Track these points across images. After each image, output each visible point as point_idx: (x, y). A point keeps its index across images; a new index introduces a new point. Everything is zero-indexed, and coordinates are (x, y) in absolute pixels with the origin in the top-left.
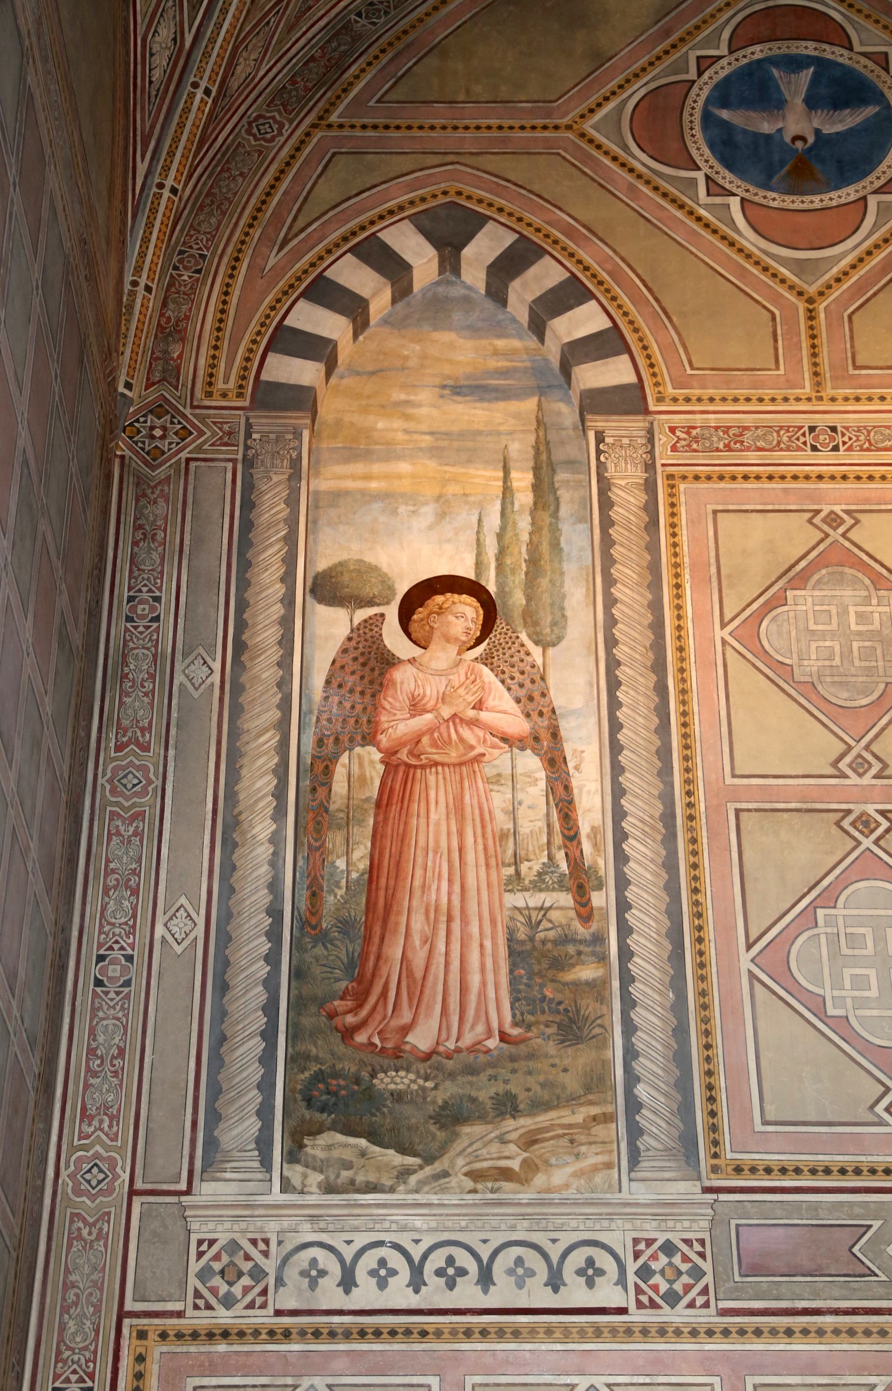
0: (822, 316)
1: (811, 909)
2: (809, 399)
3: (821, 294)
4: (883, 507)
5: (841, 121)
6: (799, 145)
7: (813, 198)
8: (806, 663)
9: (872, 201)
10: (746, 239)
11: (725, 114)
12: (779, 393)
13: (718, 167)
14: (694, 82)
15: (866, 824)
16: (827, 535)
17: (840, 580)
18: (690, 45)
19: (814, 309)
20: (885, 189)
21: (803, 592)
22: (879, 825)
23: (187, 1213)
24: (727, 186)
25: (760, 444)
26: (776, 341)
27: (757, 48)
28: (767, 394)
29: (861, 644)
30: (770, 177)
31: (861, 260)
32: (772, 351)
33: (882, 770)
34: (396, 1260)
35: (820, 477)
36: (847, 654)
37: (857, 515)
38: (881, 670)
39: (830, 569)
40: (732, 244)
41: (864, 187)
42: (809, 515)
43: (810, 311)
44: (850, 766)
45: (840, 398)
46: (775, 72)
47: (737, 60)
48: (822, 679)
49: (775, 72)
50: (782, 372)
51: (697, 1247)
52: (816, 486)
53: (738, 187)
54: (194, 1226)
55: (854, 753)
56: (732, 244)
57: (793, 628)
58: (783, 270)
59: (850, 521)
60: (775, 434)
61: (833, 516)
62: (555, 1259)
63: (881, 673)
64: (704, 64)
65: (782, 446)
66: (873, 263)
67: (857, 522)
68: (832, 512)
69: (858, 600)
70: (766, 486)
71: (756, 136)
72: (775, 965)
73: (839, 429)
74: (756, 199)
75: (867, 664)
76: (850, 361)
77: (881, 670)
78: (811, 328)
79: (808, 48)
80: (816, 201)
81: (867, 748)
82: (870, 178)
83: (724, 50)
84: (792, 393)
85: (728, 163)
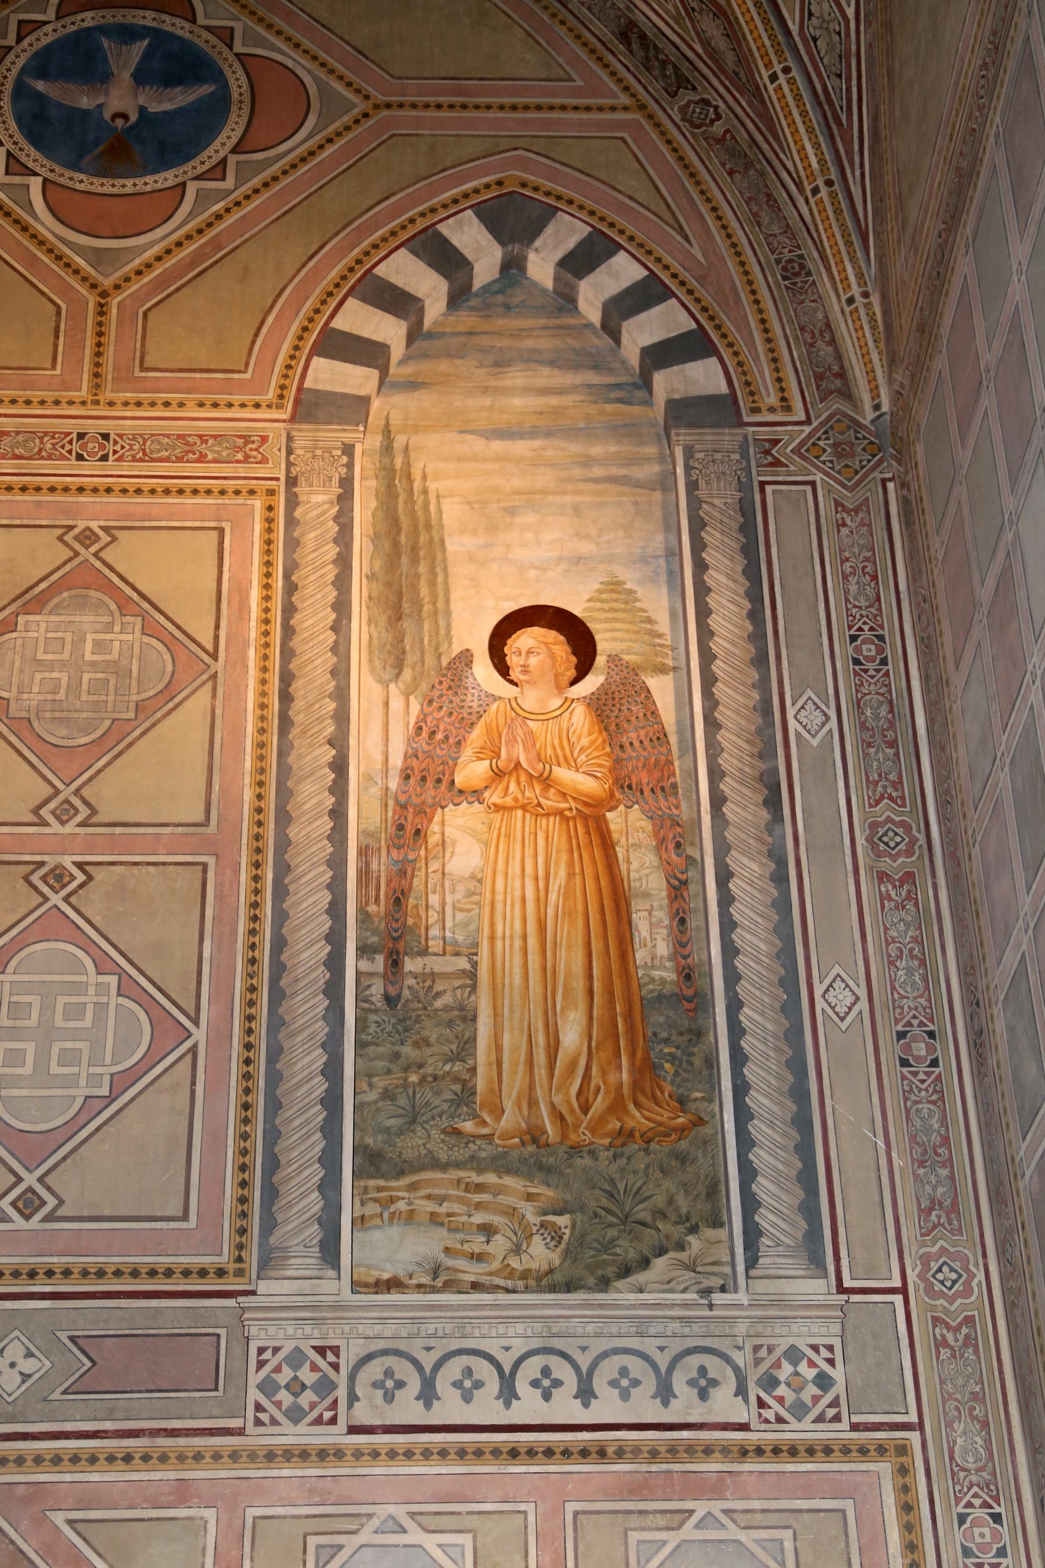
0: (114, 311)
1: (119, 971)
2: (84, 403)
3: (117, 287)
4: (147, 524)
5: (170, 99)
6: (119, 123)
7: (126, 182)
8: (25, 696)
9: (191, 189)
10: (43, 224)
11: (40, 86)
12: (49, 396)
13: (23, 142)
14: (10, 48)
15: (59, 878)
16: (77, 554)
17: (81, 605)
18: (12, 8)
19: (106, 304)
20: (209, 176)
21: (37, 618)
22: (73, 878)
23: (246, 1316)
24: (30, 164)
25: (19, 451)
26: (57, 337)
27: (89, 14)
28: (36, 396)
29: (93, 676)
30: (81, 157)
31: (168, 251)
32: (51, 349)
33: (90, 817)
34: (484, 1369)
35: (81, 490)
36: (74, 687)
37: (114, 532)
38: (110, 704)
39: (73, 592)
40: (25, 229)
41: (185, 173)
42: (60, 531)
43: (101, 305)
44: (53, 812)
45: (119, 402)
46: (105, 42)
47: (64, 27)
48: (41, 714)
49: (105, 42)
50: (58, 372)
51: (825, 1353)
52: (75, 499)
53: (42, 166)
54: (254, 1331)
55: (61, 797)
56: (25, 229)
57: (18, 658)
58: (78, 259)
59: (105, 538)
60: (37, 441)
61: (88, 533)
62: (663, 1369)
63: (110, 708)
64: (25, 29)
65: (44, 454)
66: (182, 255)
67: (114, 539)
68: (88, 528)
69: (99, 627)
70: (18, 498)
71: (73, 110)
72: (169, 1030)
73: (112, 436)
74: (61, 180)
75: (96, 698)
76: (137, 362)
77: (110, 704)
78: (100, 324)
79: (147, 18)
80: (128, 185)
81: (77, 792)
82: (192, 163)
83: (51, 14)
84: (65, 395)
85: (36, 140)
